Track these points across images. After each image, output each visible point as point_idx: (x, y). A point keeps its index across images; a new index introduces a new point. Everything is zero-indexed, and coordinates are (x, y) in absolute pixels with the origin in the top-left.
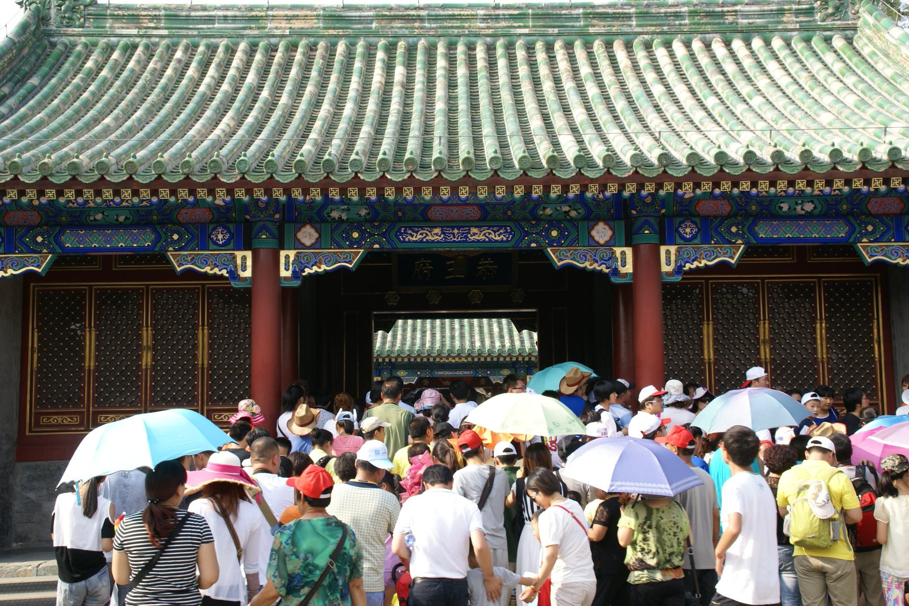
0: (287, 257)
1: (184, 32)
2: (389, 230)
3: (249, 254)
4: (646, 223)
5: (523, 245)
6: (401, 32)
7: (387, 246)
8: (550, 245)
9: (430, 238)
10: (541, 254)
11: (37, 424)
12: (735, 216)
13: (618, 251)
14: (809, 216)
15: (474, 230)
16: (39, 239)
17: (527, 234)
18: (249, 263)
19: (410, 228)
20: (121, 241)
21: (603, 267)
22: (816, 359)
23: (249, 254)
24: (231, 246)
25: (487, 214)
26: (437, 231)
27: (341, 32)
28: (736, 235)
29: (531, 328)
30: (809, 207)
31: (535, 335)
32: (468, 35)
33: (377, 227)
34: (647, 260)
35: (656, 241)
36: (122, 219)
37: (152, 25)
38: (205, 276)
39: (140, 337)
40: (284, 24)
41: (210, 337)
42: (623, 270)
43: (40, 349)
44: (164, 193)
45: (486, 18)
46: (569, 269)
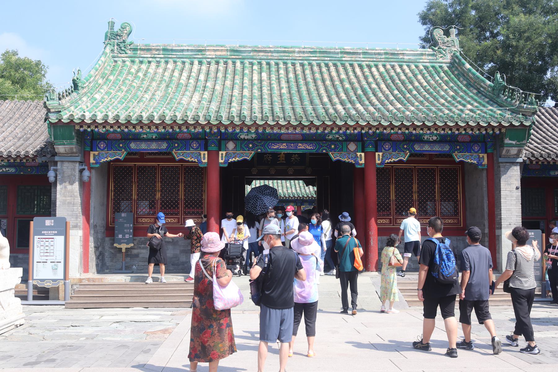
0: (222, 154)
1: (170, 56)
2: (264, 144)
3: (206, 153)
4: (370, 143)
5: (320, 151)
6: (262, 57)
7: (264, 151)
8: (331, 151)
9: (281, 147)
10: (327, 154)
11: (137, 222)
12: (406, 141)
13: (359, 154)
14: (435, 142)
15: (300, 144)
16: (121, 145)
17: (322, 146)
18: (206, 156)
19: (274, 143)
20: (154, 146)
21: (352, 161)
22: (184, 183)
23: (206, 153)
24: (199, 149)
25: (305, 139)
26: (285, 144)
27: (237, 57)
28: (406, 149)
29: (313, 186)
30: (435, 138)
31: (315, 188)
32: (292, 60)
33: (260, 143)
34: (370, 157)
35: (374, 150)
36: (154, 137)
37: (157, 53)
38: (188, 161)
39: (155, 186)
40: (213, 53)
41: (184, 187)
42: (361, 162)
43: (114, 190)
44: (108, 128)
45: (299, 52)
46: (339, 161)
